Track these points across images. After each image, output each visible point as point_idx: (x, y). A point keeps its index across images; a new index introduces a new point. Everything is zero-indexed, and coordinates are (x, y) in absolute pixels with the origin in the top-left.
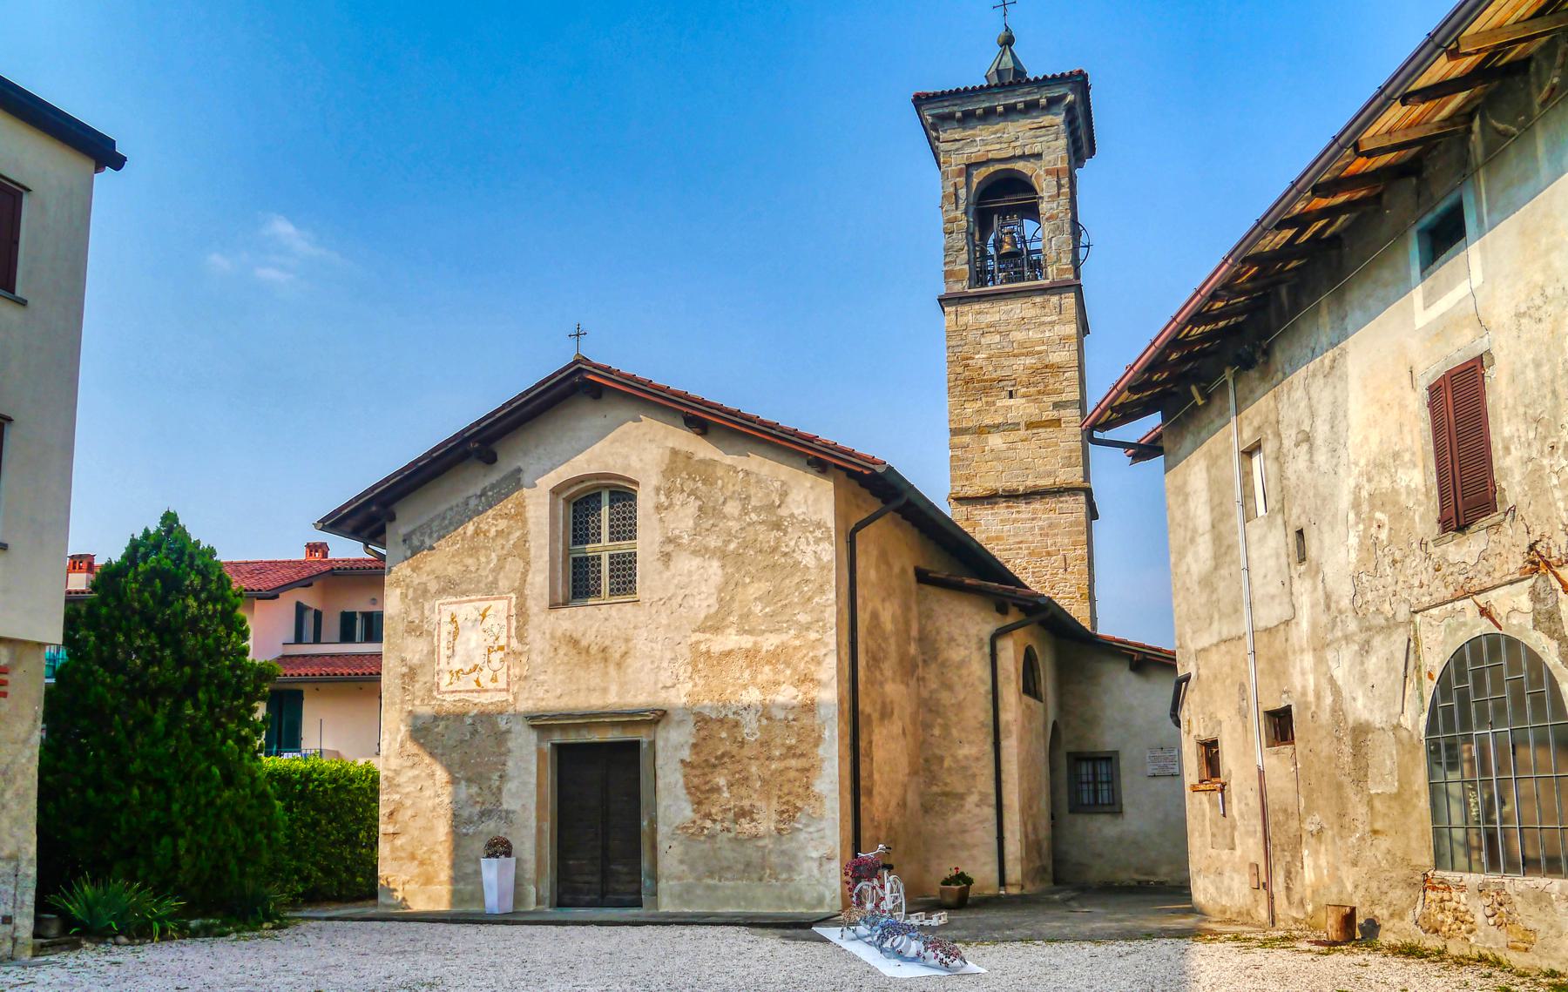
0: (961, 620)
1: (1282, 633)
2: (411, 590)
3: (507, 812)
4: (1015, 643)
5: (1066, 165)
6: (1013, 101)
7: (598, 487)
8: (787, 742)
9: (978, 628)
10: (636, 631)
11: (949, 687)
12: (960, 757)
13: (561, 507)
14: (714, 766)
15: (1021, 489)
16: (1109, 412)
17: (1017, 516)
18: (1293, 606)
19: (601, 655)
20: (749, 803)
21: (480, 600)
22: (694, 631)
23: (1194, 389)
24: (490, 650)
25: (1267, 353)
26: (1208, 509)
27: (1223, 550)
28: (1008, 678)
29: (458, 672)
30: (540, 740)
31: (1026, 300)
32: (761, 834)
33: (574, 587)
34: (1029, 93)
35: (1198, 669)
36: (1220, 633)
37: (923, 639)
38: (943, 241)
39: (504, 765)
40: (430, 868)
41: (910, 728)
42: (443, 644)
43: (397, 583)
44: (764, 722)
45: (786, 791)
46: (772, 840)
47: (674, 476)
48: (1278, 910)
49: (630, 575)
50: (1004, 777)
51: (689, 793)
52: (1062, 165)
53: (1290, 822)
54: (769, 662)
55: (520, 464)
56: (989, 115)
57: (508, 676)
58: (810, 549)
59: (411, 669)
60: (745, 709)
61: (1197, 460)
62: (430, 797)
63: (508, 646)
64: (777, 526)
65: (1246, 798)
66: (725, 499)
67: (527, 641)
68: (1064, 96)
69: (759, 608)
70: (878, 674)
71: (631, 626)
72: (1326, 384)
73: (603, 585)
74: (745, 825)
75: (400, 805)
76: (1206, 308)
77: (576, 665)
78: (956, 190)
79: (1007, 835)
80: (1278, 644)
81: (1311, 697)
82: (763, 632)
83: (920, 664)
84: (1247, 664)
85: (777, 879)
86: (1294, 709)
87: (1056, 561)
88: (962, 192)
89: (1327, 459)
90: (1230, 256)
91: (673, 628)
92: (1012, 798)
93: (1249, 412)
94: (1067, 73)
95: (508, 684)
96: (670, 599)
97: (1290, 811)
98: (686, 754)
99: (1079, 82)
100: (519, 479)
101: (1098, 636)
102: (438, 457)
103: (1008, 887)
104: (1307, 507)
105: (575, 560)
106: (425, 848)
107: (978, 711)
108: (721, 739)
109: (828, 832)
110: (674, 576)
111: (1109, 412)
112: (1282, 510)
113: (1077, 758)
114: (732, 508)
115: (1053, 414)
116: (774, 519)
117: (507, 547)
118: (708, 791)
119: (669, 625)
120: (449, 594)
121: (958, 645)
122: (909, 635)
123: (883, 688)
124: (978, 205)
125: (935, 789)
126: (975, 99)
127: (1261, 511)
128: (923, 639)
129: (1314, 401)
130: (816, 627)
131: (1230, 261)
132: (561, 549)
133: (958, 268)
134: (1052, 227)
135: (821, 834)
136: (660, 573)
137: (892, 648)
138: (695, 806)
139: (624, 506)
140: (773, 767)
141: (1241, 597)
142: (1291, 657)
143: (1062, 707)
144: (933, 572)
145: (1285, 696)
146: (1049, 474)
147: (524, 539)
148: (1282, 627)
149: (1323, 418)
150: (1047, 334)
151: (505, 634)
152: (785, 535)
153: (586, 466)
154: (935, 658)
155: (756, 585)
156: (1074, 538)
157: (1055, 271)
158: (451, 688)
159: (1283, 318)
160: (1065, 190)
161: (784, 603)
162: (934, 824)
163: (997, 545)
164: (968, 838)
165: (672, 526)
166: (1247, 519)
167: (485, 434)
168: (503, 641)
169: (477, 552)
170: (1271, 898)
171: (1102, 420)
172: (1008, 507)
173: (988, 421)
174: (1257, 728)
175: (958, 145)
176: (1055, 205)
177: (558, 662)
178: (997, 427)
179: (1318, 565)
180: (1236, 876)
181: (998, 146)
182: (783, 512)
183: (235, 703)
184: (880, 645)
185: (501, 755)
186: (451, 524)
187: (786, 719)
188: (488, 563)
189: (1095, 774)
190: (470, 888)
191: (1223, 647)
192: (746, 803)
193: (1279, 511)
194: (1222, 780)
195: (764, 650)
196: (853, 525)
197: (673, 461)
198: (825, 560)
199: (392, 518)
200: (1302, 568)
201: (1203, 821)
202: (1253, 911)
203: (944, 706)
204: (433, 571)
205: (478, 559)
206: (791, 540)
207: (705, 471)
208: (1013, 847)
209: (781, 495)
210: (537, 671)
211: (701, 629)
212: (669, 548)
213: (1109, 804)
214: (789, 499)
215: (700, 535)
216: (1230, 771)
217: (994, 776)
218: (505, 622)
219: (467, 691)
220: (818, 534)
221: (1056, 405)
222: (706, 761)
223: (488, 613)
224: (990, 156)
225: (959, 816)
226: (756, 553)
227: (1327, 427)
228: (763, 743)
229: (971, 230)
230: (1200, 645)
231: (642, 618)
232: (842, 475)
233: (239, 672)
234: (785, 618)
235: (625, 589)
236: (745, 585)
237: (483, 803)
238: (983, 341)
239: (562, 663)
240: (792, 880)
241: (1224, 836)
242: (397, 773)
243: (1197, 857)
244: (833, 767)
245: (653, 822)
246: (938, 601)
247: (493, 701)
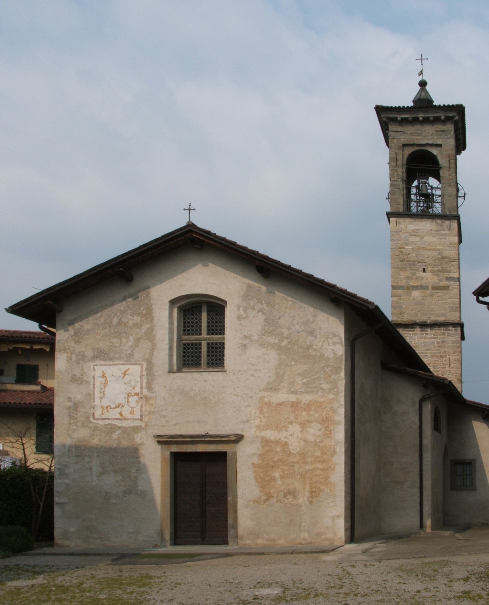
8: (316, 454)
14: (273, 467)
22: (261, 391)
24: (129, 395)
29: (107, 407)
43: (65, 350)
44: (302, 443)
49: (220, 356)
54: (305, 410)
57: (141, 411)
59: (75, 404)
60: (291, 435)
63: (141, 393)
64: (311, 333)
66: (280, 316)
88: (400, 157)
92: (427, 484)
95: (141, 416)
98: (256, 460)
99: (460, 110)
105: (184, 344)
108: (277, 452)
115: (444, 283)
120: (101, 359)
138: (261, 489)
146: (444, 315)
150: (443, 241)
151: (139, 386)
152: (315, 339)
158: (103, 416)
168: (138, 390)
171: (484, 291)
173: (412, 283)
178: (416, 288)
187: (315, 441)
195: (303, 403)
205: (121, 340)
211: (266, 390)
212: (246, 342)
218: (139, 379)
219: (114, 419)
220: (335, 340)
221: (448, 279)
223: (127, 373)
226: (298, 348)
245: (235, 497)
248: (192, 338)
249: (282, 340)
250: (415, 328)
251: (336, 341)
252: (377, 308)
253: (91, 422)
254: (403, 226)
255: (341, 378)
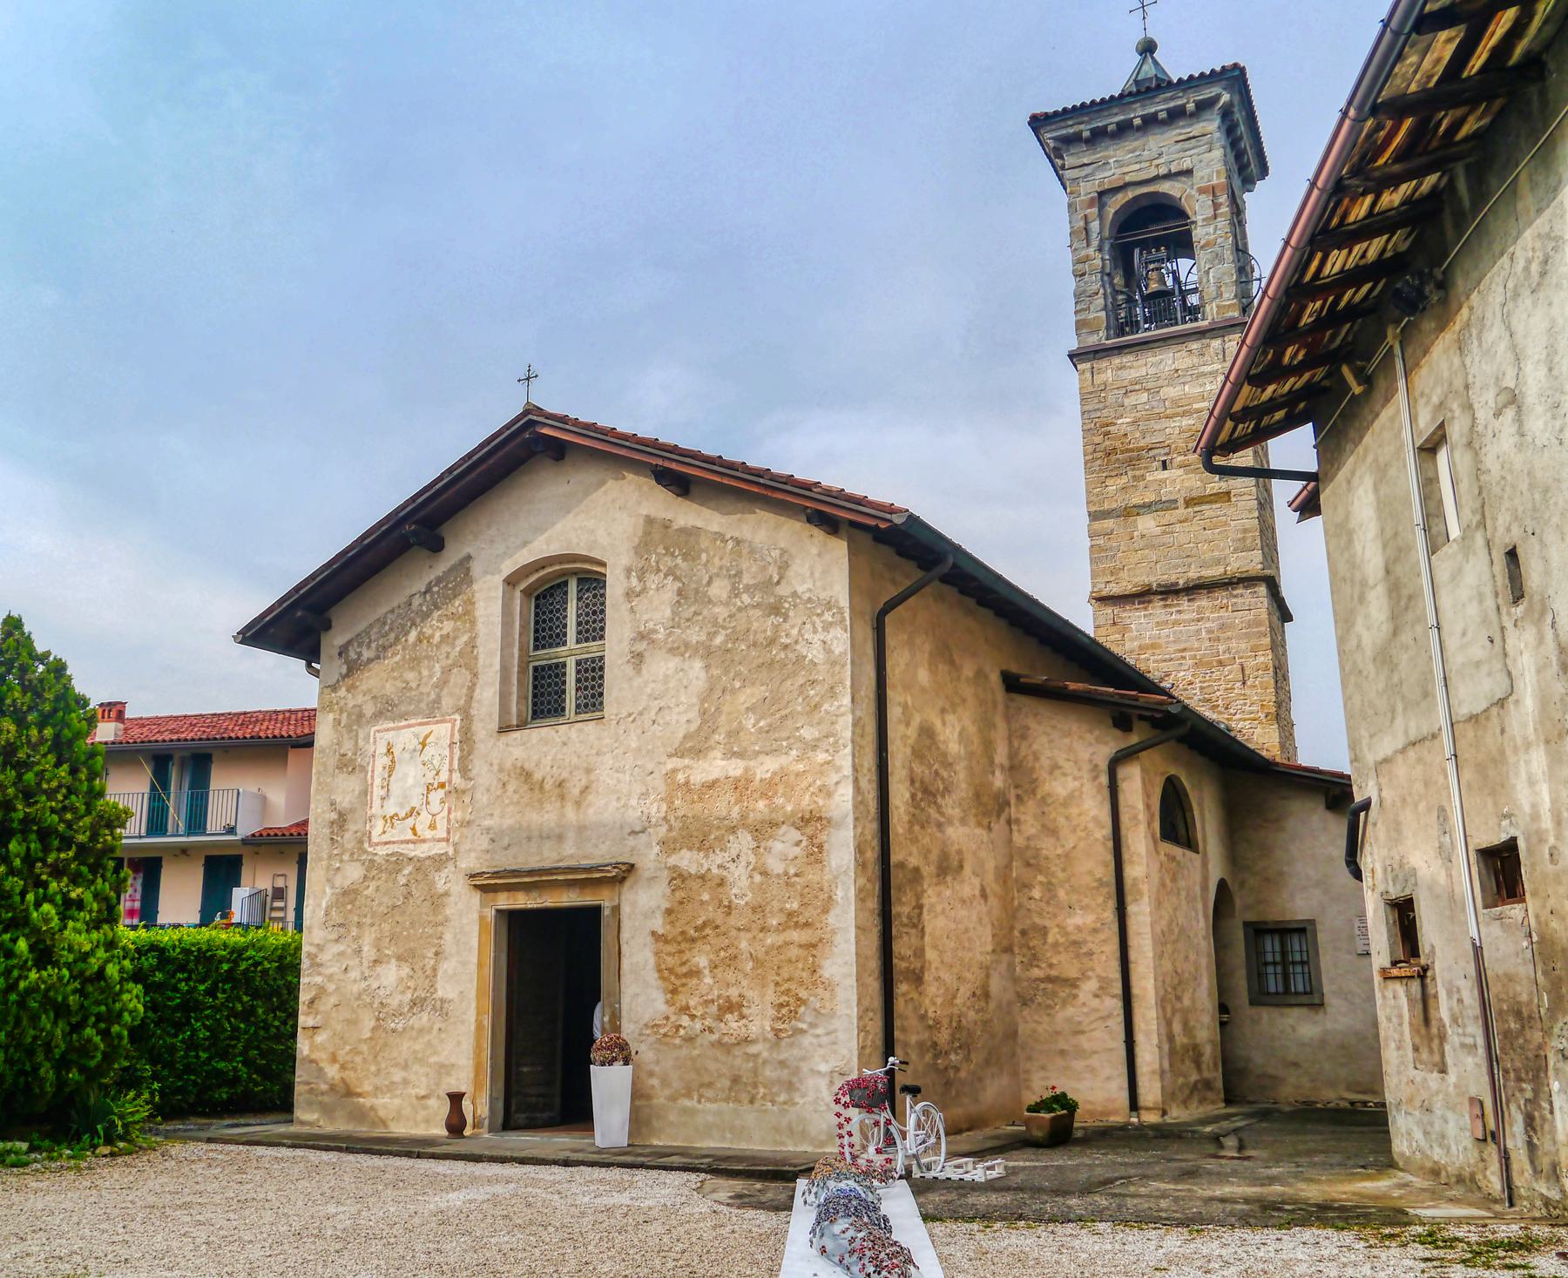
0: (1067, 741)
1: (1495, 720)
2: (345, 715)
3: (442, 1001)
4: (1144, 770)
5: (1223, 180)
6: (1153, 110)
7: (564, 573)
8: (788, 906)
9: (1091, 750)
10: (600, 758)
11: (1052, 831)
12: (1070, 929)
13: (518, 602)
14: (693, 940)
15: (1181, 582)
16: (1229, 424)
17: (1178, 617)
18: (1509, 674)
19: (557, 791)
20: (737, 993)
21: (421, 724)
22: (670, 756)
23: (1345, 370)
25: (1444, 285)
26: (1380, 545)
27: (1403, 604)
28: (1135, 818)
29: (392, 818)
30: (482, 905)
31: (1179, 347)
32: (753, 1036)
33: (535, 704)
34: (1172, 98)
35: (1380, 790)
36: (1406, 733)
37: (1015, 767)
38: (1071, 284)
39: (441, 938)
40: (352, 1074)
41: (993, 887)
42: (378, 782)
44: (758, 878)
45: (786, 976)
46: (767, 1045)
47: (648, 552)
48: (1518, 1181)
50: (1132, 955)
51: (663, 978)
52: (1219, 180)
53: (1528, 1032)
54: (764, 795)
55: (468, 550)
56: (1124, 129)
57: (449, 821)
58: (816, 639)
59: (341, 814)
61: (1361, 478)
62: (355, 981)
64: (775, 610)
65: (1459, 991)
66: (711, 578)
67: (471, 775)
68: (1218, 97)
69: (752, 721)
70: (932, 811)
71: (594, 752)
72: (1535, 304)
73: (568, 701)
74: (732, 1023)
75: (321, 991)
76: (1335, 221)
77: (527, 805)
78: (1086, 223)
79: (1140, 1038)
80: (1490, 740)
81: (1547, 823)
82: (758, 753)
83: (1013, 801)
84: (1446, 777)
85: (773, 1102)
86: (1521, 844)
87: (1230, 672)
88: (1095, 226)
89: (1546, 423)
90: (1350, 103)
91: (644, 752)
92: (1145, 985)
93: (1423, 378)
94: (1218, 69)
95: (448, 833)
96: (641, 714)
97: (1525, 1014)
98: (658, 924)
99: (1235, 77)
100: (468, 569)
101: (1301, 768)
102: (369, 545)
103: (1143, 1112)
104: (1520, 509)
105: (536, 669)
106: (348, 1048)
107: (1096, 865)
108: (702, 903)
109: (841, 1036)
110: (646, 683)
111: (1229, 424)
112: (1482, 524)
113: (1258, 931)
114: (719, 589)
116: (772, 600)
117: (452, 656)
118: (685, 975)
119: (639, 749)
120: (386, 719)
121: (1064, 775)
122: (992, 762)
123: (943, 832)
124: (1117, 239)
125: (1036, 972)
126: (1105, 113)
127: (1455, 532)
128: (1015, 767)
129: (1518, 337)
130: (824, 745)
131: (1352, 112)
132: (516, 655)
133: (1092, 316)
134: (1209, 256)
135: (832, 1037)
136: (631, 679)
137: (961, 776)
138: (669, 996)
139: (595, 596)
140: (769, 941)
141: (1431, 671)
142: (1512, 759)
143: (1234, 857)
144: (1026, 676)
145: (1505, 823)
146: (1218, 562)
147: (472, 645)
148: (1494, 711)
149: (1536, 357)
151: (447, 766)
152: (785, 621)
153: (545, 547)
154: (1034, 792)
155: (748, 691)
156: (1253, 642)
157: (1215, 310)
158: (385, 838)
159: (1460, 221)
160: (1224, 209)
161: (783, 712)
162: (1036, 1022)
163: (1153, 654)
164: (1083, 1041)
165: (645, 617)
166: (1433, 549)
167: (422, 513)
168: (444, 777)
169: (418, 664)
170: (1505, 1158)
171: (1223, 436)
172: (1165, 606)
173: (1136, 500)
174: (1466, 879)
175: (1088, 170)
176: (1211, 229)
177: (507, 802)
178: (1147, 507)
179: (1543, 601)
180: (1450, 1115)
181: (1137, 167)
182: (783, 590)
183: (63, 855)
184: (937, 773)
185: (437, 925)
186: (391, 629)
187: (786, 874)
188: (431, 676)
189: (1284, 953)
190: (397, 1101)
191: (1411, 754)
192: (733, 993)
193: (1478, 527)
194: (1423, 961)
195: (758, 778)
196: (881, 606)
197: (647, 533)
198: (837, 652)
199: (328, 626)
200: (1519, 610)
201: (1401, 1025)
202: (1479, 1177)
203: (1047, 858)
204: (370, 691)
205: (420, 673)
206: (793, 627)
207: (687, 542)
208: (1148, 1056)
209: (780, 568)
210: (482, 814)
211: (679, 753)
212: (641, 646)
213: (1305, 993)
214: (790, 573)
215: (679, 627)
216: (1433, 947)
217: (1118, 954)
218: (447, 752)
219: (402, 842)
220: (828, 617)
222: (683, 933)
224: (1128, 179)
225: (1070, 1011)
226: (749, 647)
227: (1542, 372)
228: (757, 909)
229: (1108, 270)
230: (1380, 756)
231: (607, 741)
232: (865, 539)
233: (69, 816)
234: (784, 734)
235: (594, 705)
236: (734, 691)
237: (415, 989)
238: (1127, 402)
239: (512, 803)
240: (794, 1104)
241: (1431, 1051)
242: (320, 947)
243: (1395, 1080)
244: (847, 941)
246: (1035, 715)
247: (430, 854)
248: (547, 656)
249: (716, 633)
250: (1150, 602)
251: (830, 619)
252: (913, 520)
253: (366, 852)
254: (1108, 376)
255: (843, 709)
